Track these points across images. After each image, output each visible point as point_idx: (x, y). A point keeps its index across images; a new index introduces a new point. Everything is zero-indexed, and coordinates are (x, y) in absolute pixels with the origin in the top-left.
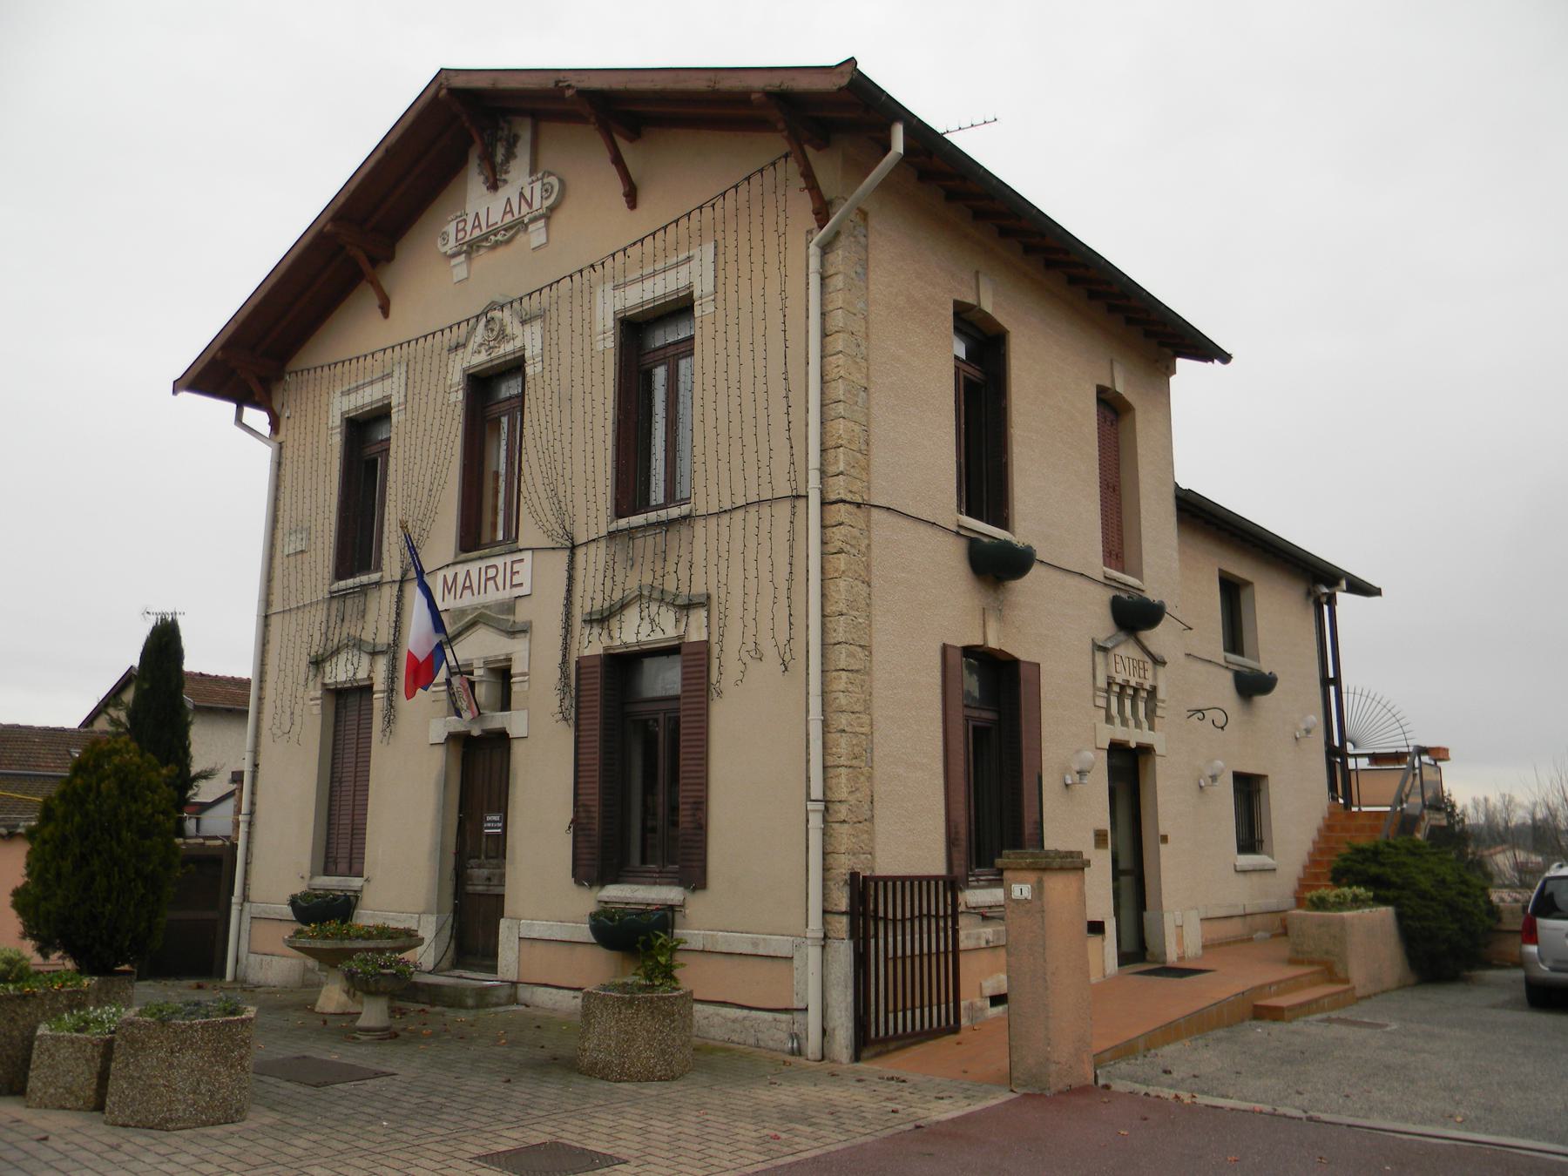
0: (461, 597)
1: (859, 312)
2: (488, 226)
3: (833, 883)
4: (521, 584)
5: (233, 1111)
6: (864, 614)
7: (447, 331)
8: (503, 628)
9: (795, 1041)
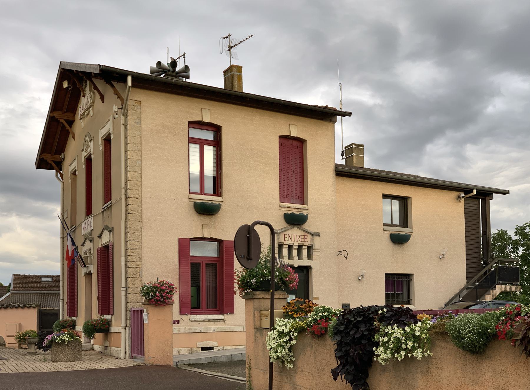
7: (288, 179)
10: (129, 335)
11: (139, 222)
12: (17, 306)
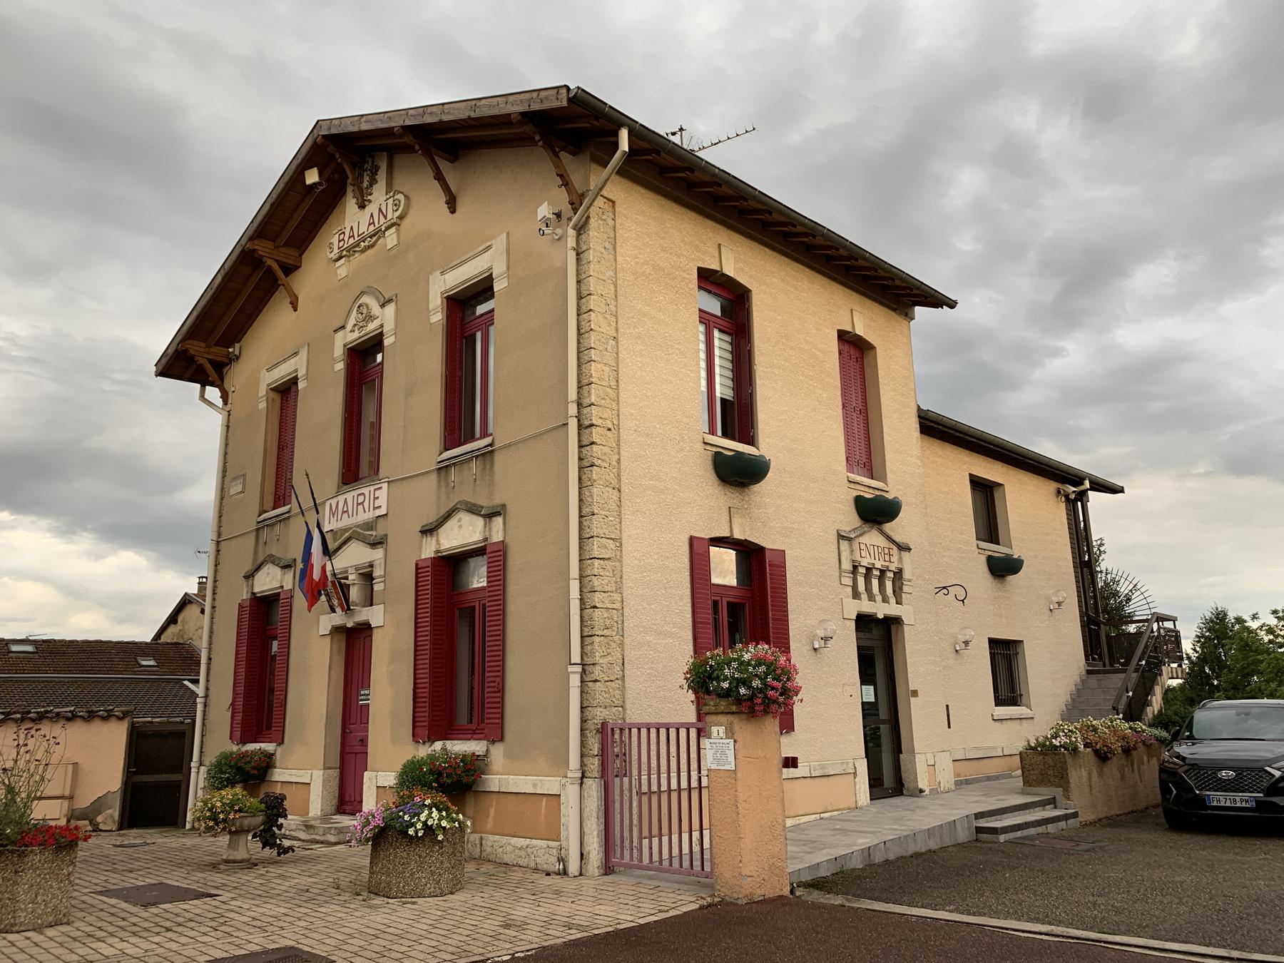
0: (341, 519)
1: (608, 279)
2: (359, 236)
3: (588, 731)
4: (380, 507)
5: (61, 916)
6: (615, 514)
8: (367, 542)
9: (561, 863)
10: (600, 803)
11: (614, 489)
12: (70, 714)
